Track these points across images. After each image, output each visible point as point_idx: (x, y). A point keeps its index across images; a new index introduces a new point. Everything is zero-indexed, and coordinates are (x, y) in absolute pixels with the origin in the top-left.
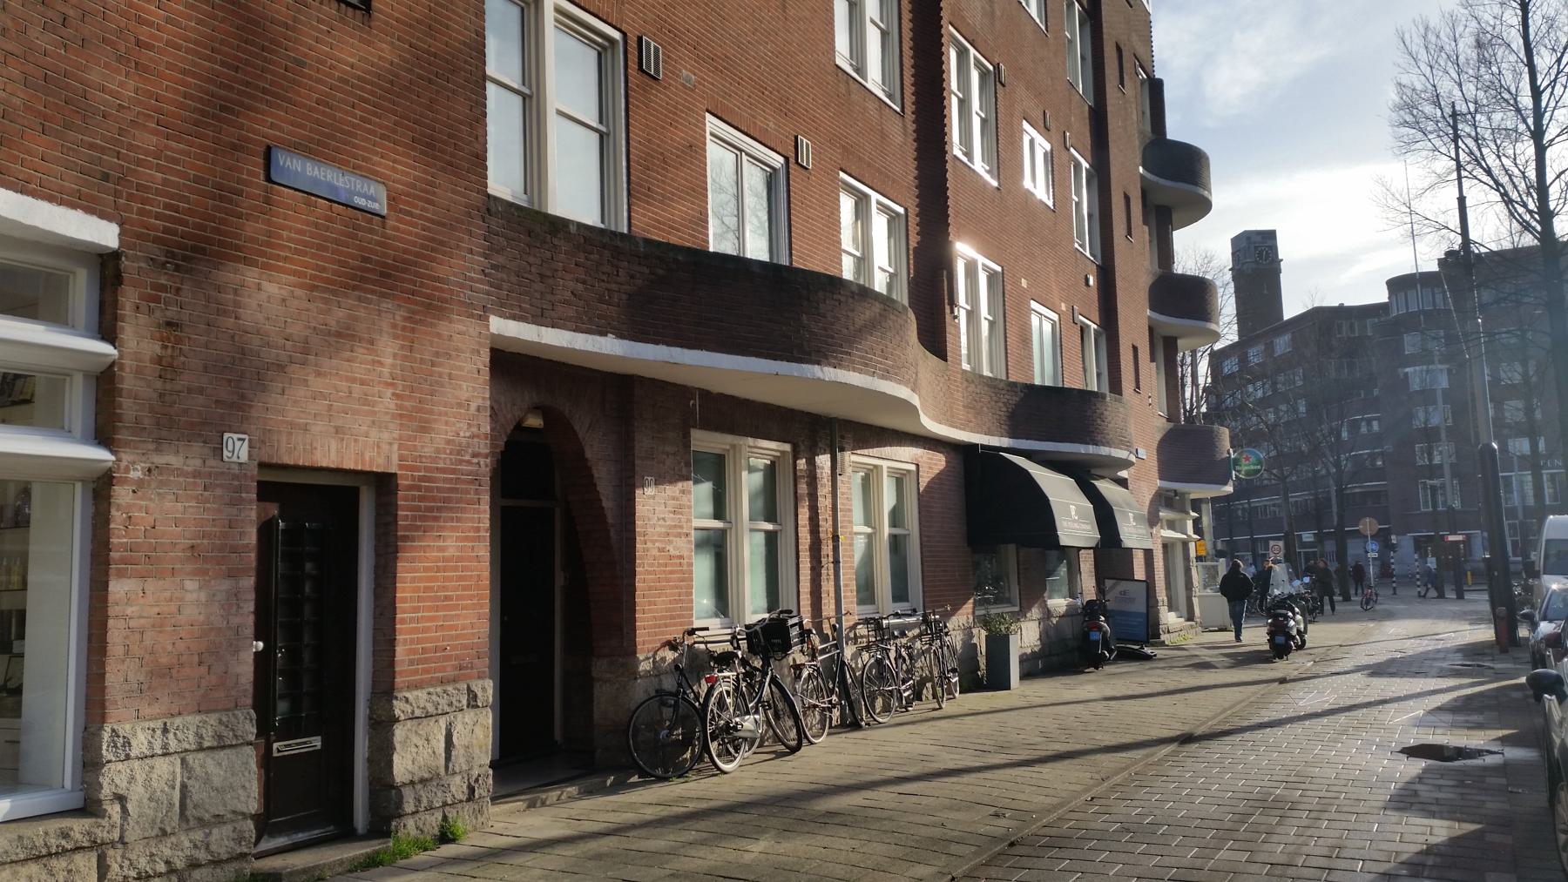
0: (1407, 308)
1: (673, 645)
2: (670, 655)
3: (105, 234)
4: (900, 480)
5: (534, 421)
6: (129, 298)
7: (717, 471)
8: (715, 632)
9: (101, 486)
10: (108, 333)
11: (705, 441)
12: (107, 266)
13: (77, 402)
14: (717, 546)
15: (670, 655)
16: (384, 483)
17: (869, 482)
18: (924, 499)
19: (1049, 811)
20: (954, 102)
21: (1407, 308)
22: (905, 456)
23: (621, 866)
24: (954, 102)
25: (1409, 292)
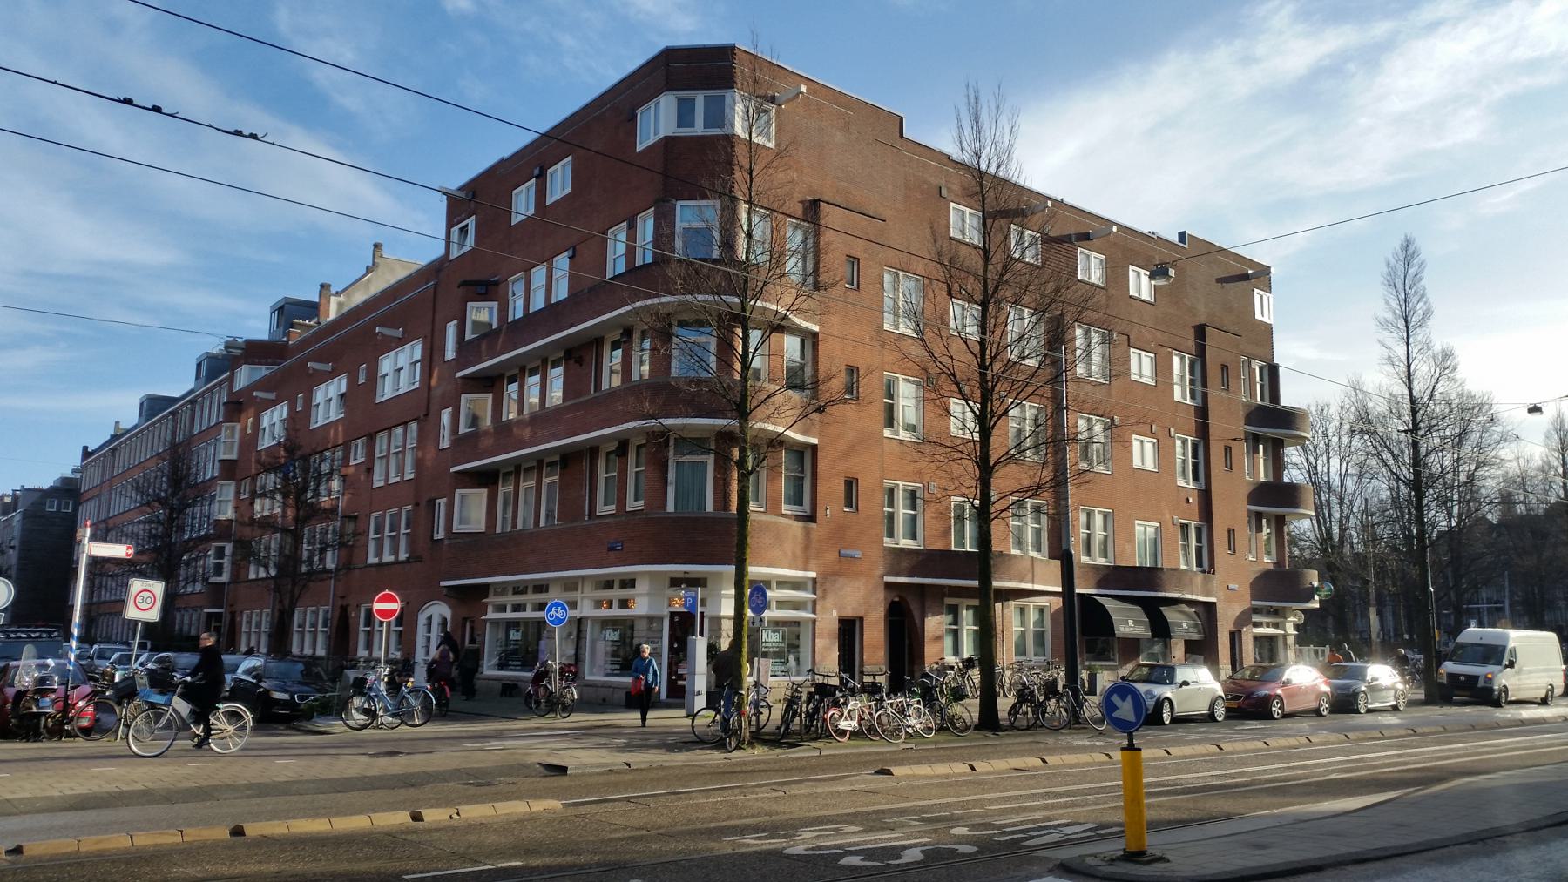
0: (1241, 440)
1: (937, 663)
2: (935, 666)
3: (813, 575)
4: (1041, 610)
5: (897, 599)
6: (818, 585)
7: (954, 611)
8: (950, 659)
9: (814, 621)
10: (815, 594)
11: (949, 601)
12: (814, 580)
13: (810, 606)
14: (956, 634)
15: (935, 666)
16: (861, 619)
17: (1022, 610)
18: (1053, 616)
19: (1158, 806)
20: (475, 812)
21: (1241, 440)
22: (1042, 601)
23: (1072, 455)
24: (475, 812)
25: (482, 527)
